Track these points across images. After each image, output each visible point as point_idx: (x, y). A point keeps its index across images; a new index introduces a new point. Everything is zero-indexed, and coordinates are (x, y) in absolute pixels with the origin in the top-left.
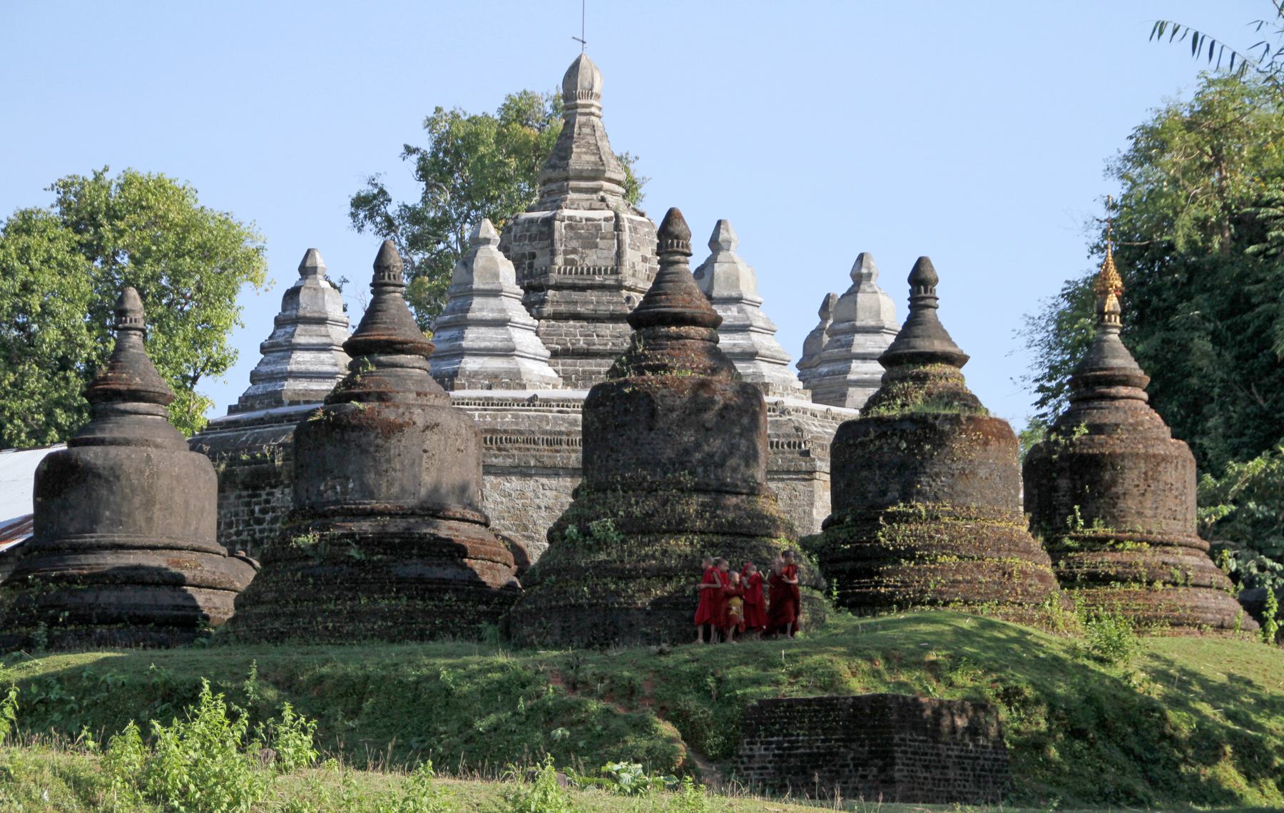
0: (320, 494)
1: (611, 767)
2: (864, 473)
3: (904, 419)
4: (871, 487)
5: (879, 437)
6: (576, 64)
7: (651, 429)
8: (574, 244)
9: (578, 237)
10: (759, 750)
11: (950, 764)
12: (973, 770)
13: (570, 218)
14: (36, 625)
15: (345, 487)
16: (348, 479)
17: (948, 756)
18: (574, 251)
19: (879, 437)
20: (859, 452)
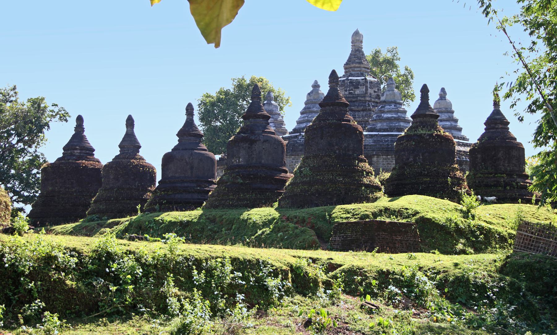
0: (233, 163)
1: (103, 230)
2: (403, 153)
3: (415, 135)
4: (405, 157)
5: (407, 141)
6: (152, 5)
7: (322, 139)
8: (352, 87)
9: (353, 85)
10: (337, 239)
11: (396, 242)
12: (406, 244)
13: (351, 79)
14: (156, 205)
15: (239, 161)
16: (240, 158)
17: (397, 240)
18: (352, 90)
19: (407, 141)
20: (401, 146)
